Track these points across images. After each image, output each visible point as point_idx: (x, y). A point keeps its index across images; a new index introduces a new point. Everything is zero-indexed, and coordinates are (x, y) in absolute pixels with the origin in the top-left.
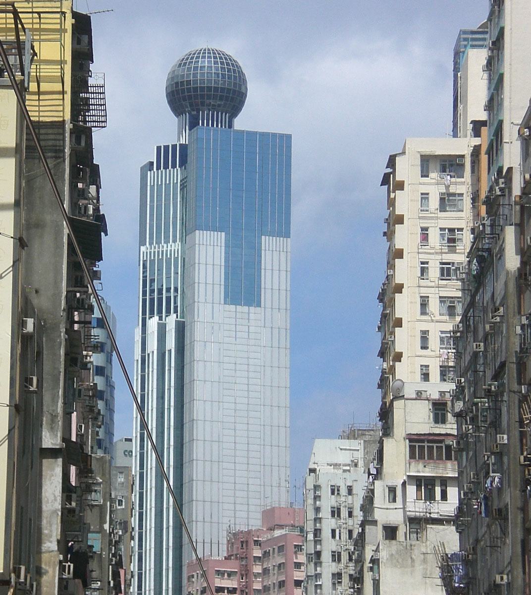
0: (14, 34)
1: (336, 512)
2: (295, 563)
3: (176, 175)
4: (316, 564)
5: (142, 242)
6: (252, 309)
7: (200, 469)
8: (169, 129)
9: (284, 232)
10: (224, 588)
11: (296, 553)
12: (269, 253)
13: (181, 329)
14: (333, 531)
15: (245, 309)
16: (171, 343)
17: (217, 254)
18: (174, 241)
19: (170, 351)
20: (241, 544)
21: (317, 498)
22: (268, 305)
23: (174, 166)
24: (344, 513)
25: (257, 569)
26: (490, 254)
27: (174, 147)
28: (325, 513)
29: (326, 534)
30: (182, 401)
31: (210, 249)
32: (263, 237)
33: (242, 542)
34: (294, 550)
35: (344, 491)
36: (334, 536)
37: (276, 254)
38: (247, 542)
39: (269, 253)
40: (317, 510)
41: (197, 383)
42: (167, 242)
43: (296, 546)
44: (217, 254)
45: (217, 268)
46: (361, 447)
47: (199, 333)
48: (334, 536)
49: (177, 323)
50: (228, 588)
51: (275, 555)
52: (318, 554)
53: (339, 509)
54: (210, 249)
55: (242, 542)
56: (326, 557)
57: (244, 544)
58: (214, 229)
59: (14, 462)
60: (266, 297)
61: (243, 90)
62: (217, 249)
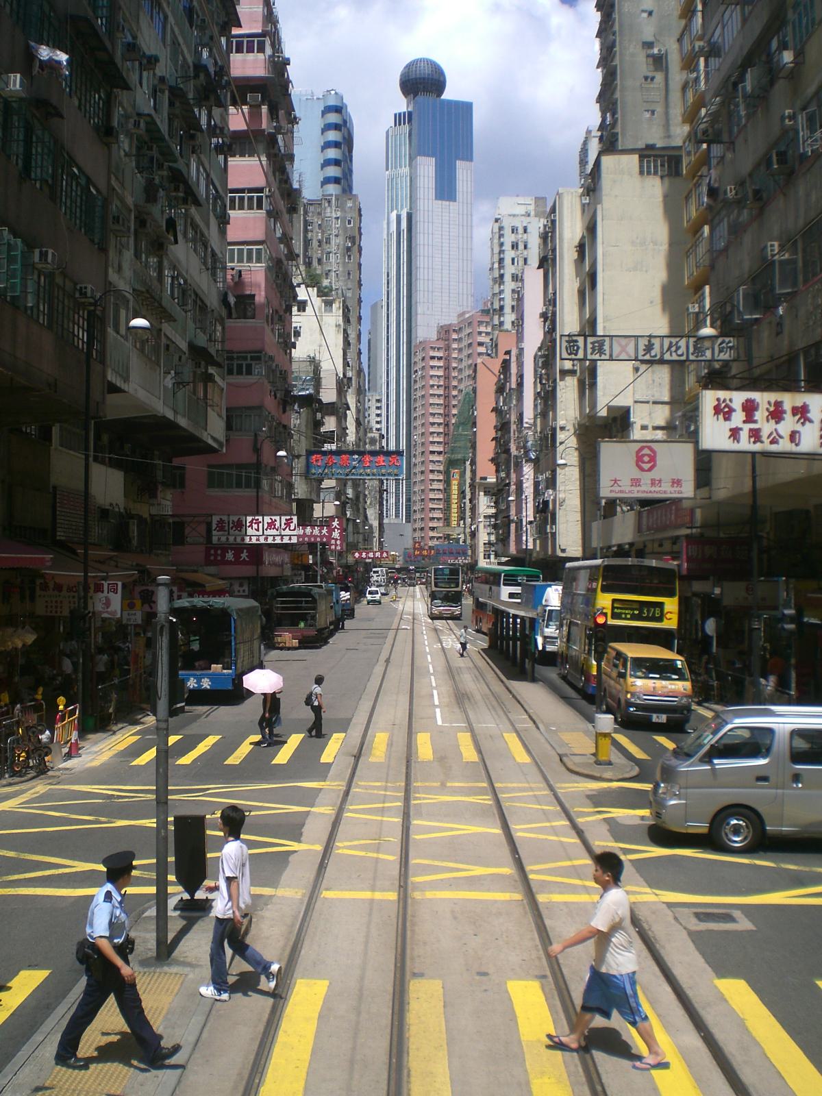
0: (413, 802)
1: (515, 246)
3: (406, 128)
4: (500, 285)
5: (387, 169)
8: (401, 104)
9: (469, 157)
13: (410, 217)
14: (513, 259)
20: (445, 332)
21: (501, 236)
24: (521, 246)
25: (455, 346)
27: (404, 113)
28: (507, 247)
29: (508, 261)
30: (407, 768)
35: (521, 230)
36: (513, 264)
40: (502, 245)
41: (419, 316)
42: (401, 167)
46: (533, 202)
47: (420, 218)
48: (513, 264)
49: (408, 213)
52: (502, 276)
53: (517, 244)
56: (508, 278)
57: (447, 332)
58: (428, 156)
60: (459, 196)
61: (442, 79)
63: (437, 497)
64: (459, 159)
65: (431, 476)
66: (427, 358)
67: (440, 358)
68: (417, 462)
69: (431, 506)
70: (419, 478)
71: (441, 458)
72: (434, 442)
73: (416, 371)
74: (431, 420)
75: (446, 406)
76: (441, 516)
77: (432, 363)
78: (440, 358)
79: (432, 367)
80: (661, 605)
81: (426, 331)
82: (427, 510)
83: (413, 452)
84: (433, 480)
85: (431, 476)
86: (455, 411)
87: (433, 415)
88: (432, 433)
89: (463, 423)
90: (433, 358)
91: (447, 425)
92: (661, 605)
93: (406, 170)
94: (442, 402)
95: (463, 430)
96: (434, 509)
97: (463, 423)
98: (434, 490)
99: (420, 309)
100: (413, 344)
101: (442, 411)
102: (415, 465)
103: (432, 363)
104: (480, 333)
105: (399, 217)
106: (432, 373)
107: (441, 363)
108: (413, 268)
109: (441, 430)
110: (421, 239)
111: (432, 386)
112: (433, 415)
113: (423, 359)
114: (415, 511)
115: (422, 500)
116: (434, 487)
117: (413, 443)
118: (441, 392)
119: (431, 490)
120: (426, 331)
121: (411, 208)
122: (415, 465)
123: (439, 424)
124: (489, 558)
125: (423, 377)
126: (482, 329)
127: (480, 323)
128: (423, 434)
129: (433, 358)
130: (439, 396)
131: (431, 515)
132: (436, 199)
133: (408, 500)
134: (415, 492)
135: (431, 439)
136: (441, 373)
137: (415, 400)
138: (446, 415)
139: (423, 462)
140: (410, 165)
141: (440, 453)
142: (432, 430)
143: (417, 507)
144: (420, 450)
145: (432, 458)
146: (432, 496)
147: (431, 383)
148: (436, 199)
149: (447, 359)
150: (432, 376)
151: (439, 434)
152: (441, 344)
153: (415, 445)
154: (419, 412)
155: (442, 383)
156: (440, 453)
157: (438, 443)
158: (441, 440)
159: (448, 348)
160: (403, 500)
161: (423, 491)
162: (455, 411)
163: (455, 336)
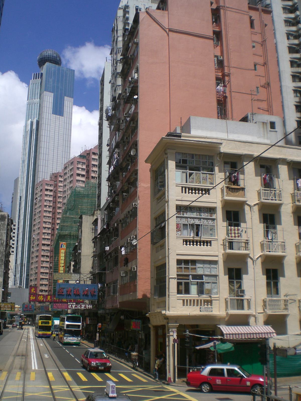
2: (77, 167)
6: (61, 117)
7: (41, 168)
10: (48, 189)
11: (78, 164)
12: (67, 102)
13: (38, 123)
15: (59, 116)
16: (34, 127)
17: (51, 99)
18: (37, 99)
19: (34, 129)
20: (55, 176)
22: (66, 116)
23: (38, 78)
25: (60, 184)
26: (80, 244)
31: (49, 97)
32: (65, 97)
33: (55, 176)
34: (77, 163)
37: (69, 102)
38: (57, 176)
39: (67, 102)
43: (78, 161)
44: (51, 99)
45: (50, 103)
50: (50, 189)
51: (69, 167)
54: (49, 97)
55: (55, 176)
57: (56, 177)
59: (34, 393)
62: (51, 98)
63: (45, 271)
64: (66, 96)
65: (42, 259)
66: (44, 190)
67: (51, 191)
68: (34, 250)
69: (41, 277)
70: (35, 260)
71: (49, 248)
72: (45, 239)
73: (37, 198)
74: (44, 225)
75: (54, 219)
76: (47, 283)
77: (47, 193)
78: (51, 191)
79: (46, 195)
80: (49, 322)
81: (44, 174)
82: (39, 279)
83: (32, 245)
84: (43, 261)
85: (42, 259)
86: (58, 221)
87: (45, 222)
88: (44, 233)
89: (70, 209)
90: (47, 190)
91: (53, 229)
92: (49, 322)
93: (37, 100)
94: (51, 215)
95: (70, 214)
96: (43, 279)
97: (70, 209)
98: (44, 267)
99: (41, 162)
100: (36, 183)
101: (50, 221)
102: (33, 252)
103: (47, 193)
104: (78, 168)
105: (32, 123)
106: (46, 198)
107: (51, 193)
108: (38, 147)
109: (50, 232)
110: (43, 133)
111: (46, 206)
112: (45, 222)
113: (41, 190)
114: (31, 280)
115: (36, 273)
116: (44, 265)
117: (32, 240)
118: (51, 209)
119: (42, 267)
120: (44, 174)
121: (39, 119)
122: (33, 252)
123: (49, 228)
124: (187, 291)
125: (40, 201)
126: (80, 166)
127: (79, 162)
128: (38, 233)
129: (47, 190)
130: (49, 212)
131: (41, 283)
132: (53, 114)
133: (28, 275)
134: (32, 269)
135: (43, 237)
136: (51, 199)
137: (35, 215)
138: (53, 224)
139: (37, 251)
140: (40, 98)
141: (48, 245)
142: (44, 231)
143: (32, 278)
144: (36, 243)
145: (44, 248)
146: (42, 270)
147: (45, 204)
148: (53, 114)
149: (55, 192)
150: (46, 200)
151: (48, 234)
152: (52, 183)
153: (33, 241)
154: (37, 221)
155: (51, 205)
156: (48, 245)
157: (48, 239)
158: (49, 237)
159: (56, 186)
160: (24, 275)
161: (37, 268)
162: (58, 221)
163: (60, 179)
